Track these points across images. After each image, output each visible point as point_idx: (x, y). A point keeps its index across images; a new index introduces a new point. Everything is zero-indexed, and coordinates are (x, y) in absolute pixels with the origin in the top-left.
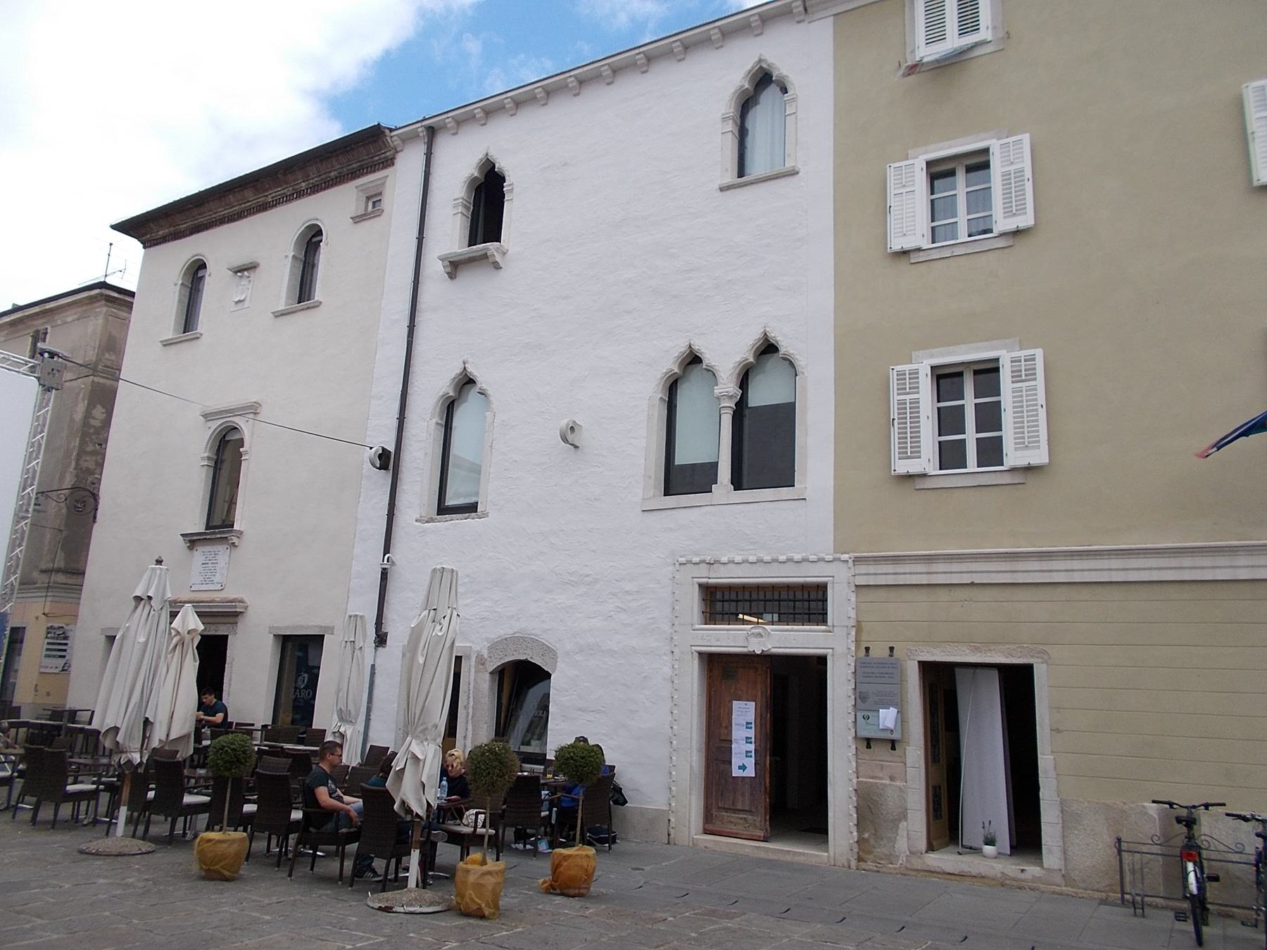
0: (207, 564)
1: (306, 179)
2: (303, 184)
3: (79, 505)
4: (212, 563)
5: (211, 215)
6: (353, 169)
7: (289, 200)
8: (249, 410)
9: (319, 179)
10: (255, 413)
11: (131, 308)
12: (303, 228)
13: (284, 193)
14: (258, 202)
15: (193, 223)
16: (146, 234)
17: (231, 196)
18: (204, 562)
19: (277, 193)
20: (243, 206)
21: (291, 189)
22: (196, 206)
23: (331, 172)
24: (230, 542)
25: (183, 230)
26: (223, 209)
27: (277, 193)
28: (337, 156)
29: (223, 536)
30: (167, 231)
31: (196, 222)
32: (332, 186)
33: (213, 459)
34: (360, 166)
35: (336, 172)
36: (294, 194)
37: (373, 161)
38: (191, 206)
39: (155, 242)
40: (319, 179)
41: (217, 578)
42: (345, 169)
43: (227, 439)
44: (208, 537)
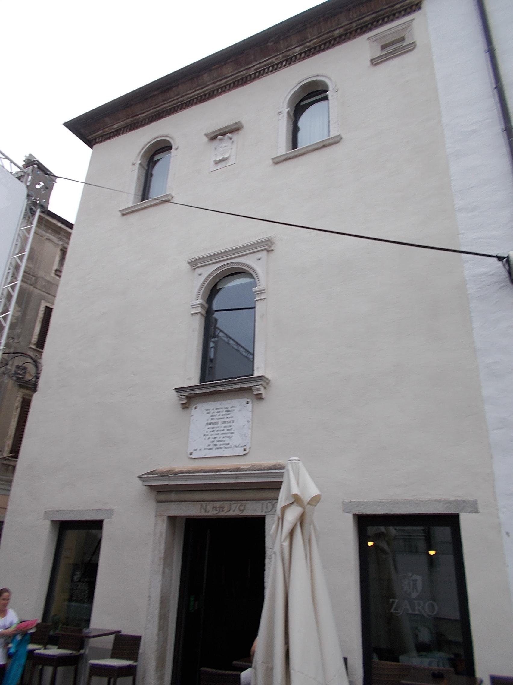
0: (217, 423)
1: (301, 43)
2: (298, 49)
3: (19, 372)
4: (224, 422)
5: (178, 99)
6: (365, 22)
7: (276, 69)
8: (262, 246)
9: (320, 39)
10: (268, 251)
11: (69, 238)
12: (298, 87)
13: (272, 62)
14: (238, 76)
15: (155, 110)
16: (98, 130)
17: (206, 75)
18: (210, 421)
19: (263, 64)
20: (218, 83)
21: (281, 56)
22: (162, 92)
23: (334, 30)
24: (255, 393)
25: (141, 120)
26: (194, 90)
27: (263, 64)
28: (348, 10)
29: (244, 386)
30: (123, 123)
31: (159, 109)
32: (334, 45)
33: (205, 307)
34: (374, 18)
35: (342, 30)
36: (283, 61)
37: (393, 10)
38: (156, 93)
39: (108, 136)
40: (320, 39)
41: (236, 440)
42: (354, 24)
43: (218, 287)
44: (220, 389)
